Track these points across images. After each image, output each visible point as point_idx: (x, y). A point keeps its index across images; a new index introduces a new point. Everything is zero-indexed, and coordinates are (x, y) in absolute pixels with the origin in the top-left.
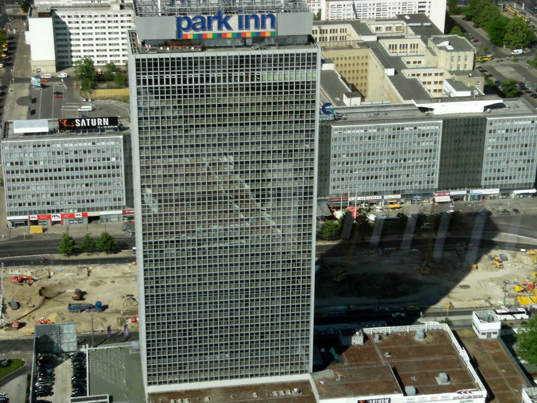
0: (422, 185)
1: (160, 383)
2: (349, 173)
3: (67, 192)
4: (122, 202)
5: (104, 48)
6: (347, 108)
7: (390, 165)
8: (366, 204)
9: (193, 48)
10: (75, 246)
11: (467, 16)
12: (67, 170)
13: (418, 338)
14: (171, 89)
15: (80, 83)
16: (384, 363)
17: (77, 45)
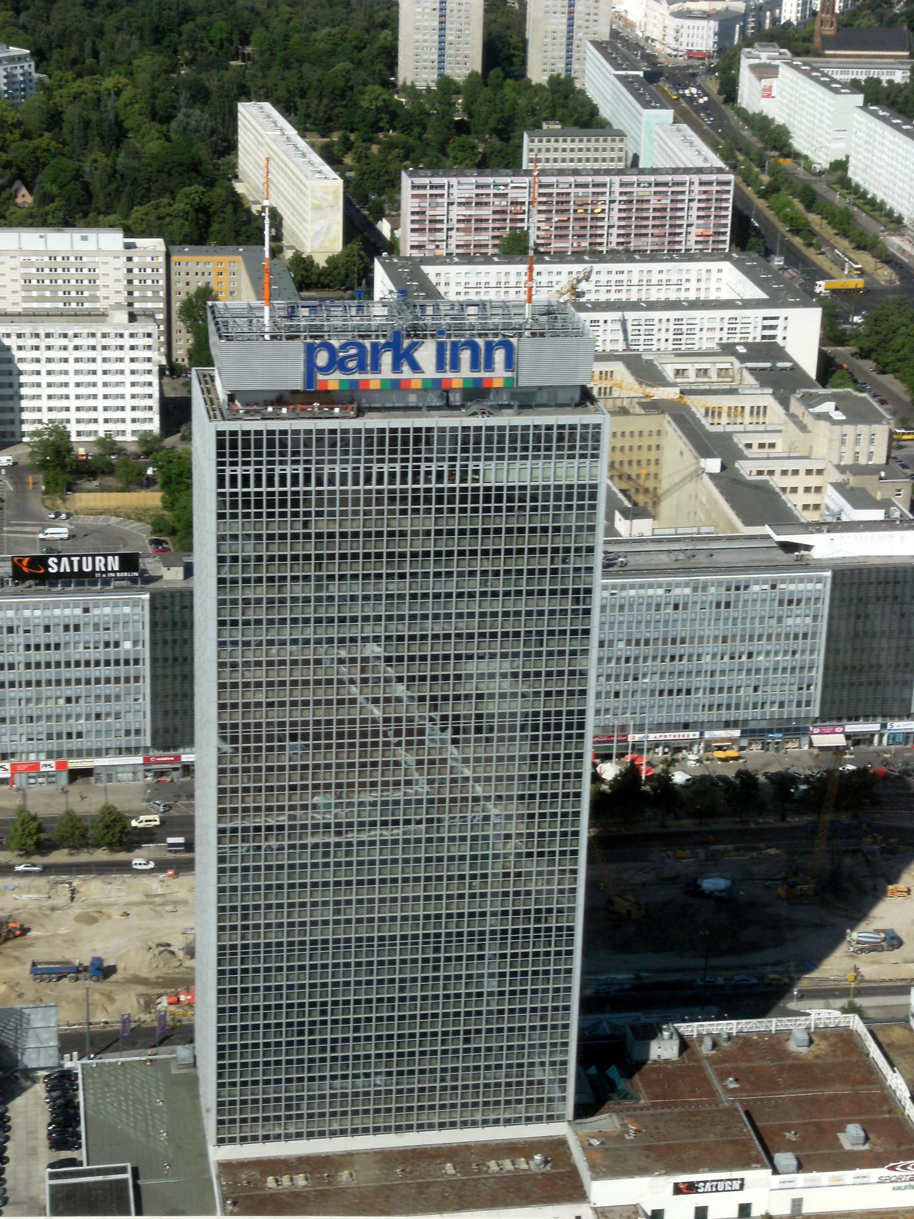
0: (786, 710)
1: (243, 1140)
2: (630, 681)
3: (25, 715)
4: (142, 737)
5: (91, 403)
6: (626, 542)
7: (719, 665)
8: (666, 750)
9: (337, 410)
10: (42, 836)
11: (861, 349)
12: (28, 666)
13: (797, 1046)
14: (338, 496)
15: (40, 477)
16: (725, 1100)
17: (34, 397)
